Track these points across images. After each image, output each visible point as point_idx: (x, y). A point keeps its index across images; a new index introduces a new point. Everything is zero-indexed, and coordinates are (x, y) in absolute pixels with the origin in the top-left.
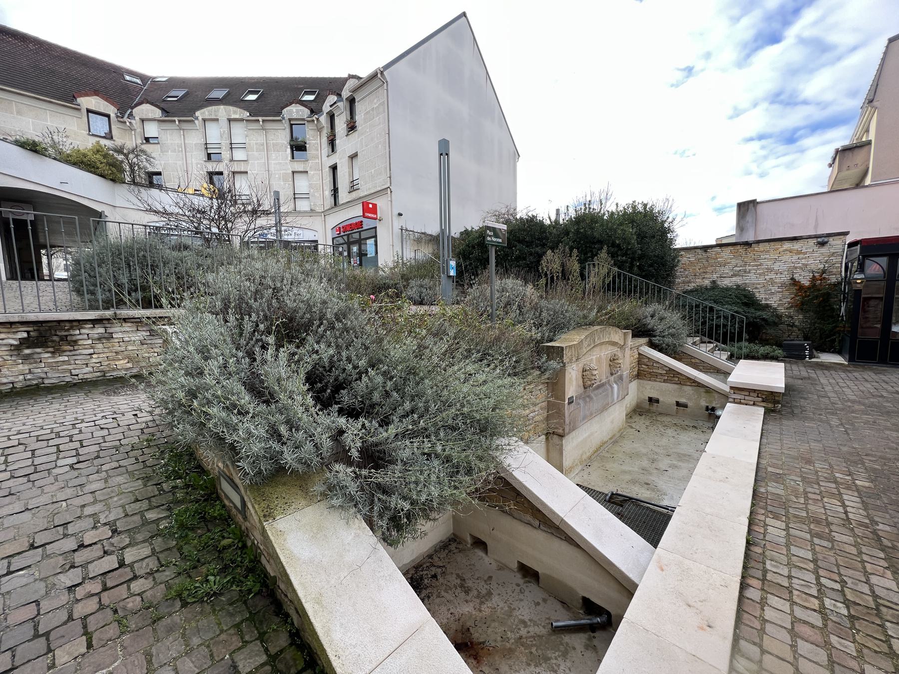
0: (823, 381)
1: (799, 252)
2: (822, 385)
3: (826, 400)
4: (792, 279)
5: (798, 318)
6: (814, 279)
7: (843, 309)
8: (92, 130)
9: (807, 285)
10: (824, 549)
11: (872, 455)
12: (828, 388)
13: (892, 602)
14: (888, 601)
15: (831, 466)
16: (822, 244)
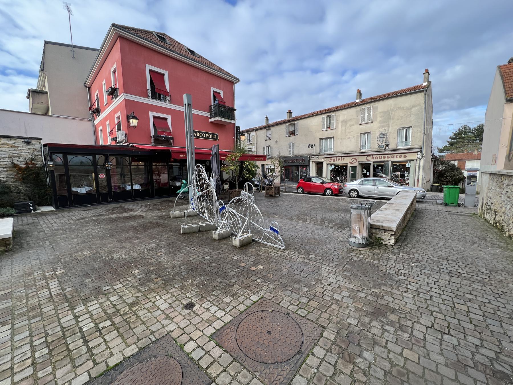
0: (41, 222)
1: (14, 146)
2: (41, 225)
3: (43, 233)
4: (13, 163)
5: (23, 188)
6: (27, 163)
7: (48, 181)
9: (23, 167)
10: (36, 323)
11: (65, 255)
12: (44, 226)
13: (70, 326)
14: (69, 326)
15: (43, 271)
16: (28, 143)
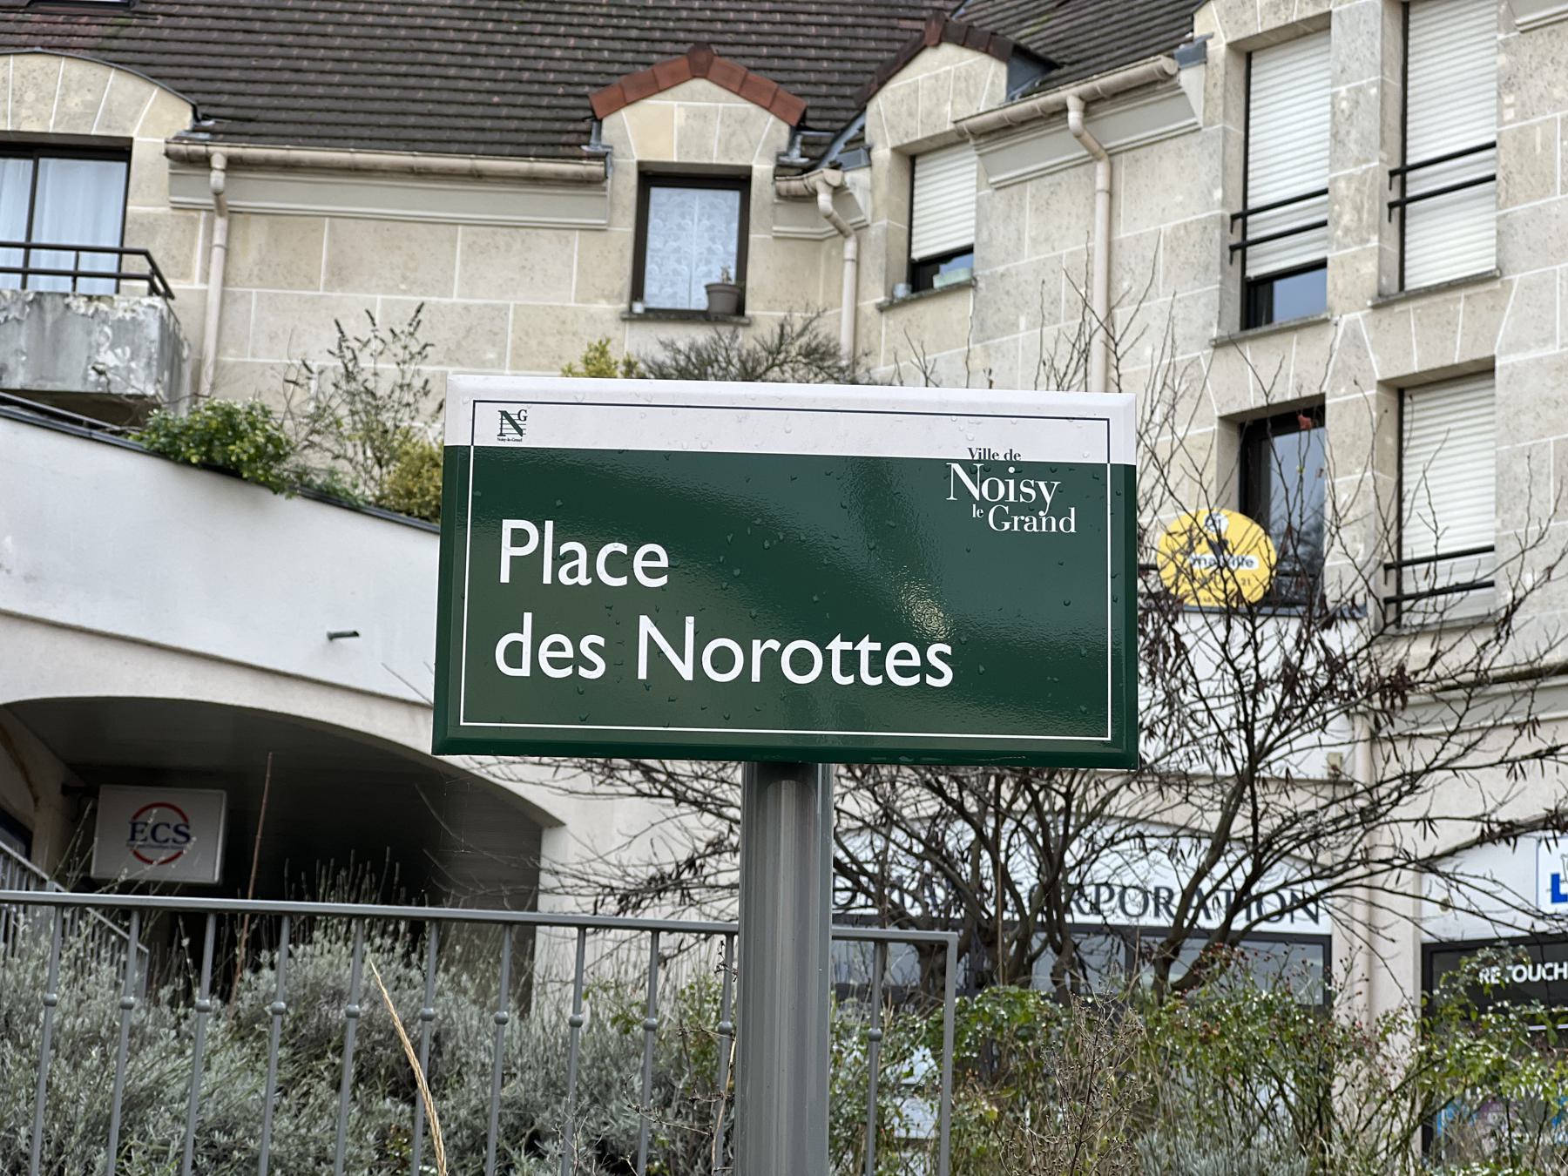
8: (650, 287)
